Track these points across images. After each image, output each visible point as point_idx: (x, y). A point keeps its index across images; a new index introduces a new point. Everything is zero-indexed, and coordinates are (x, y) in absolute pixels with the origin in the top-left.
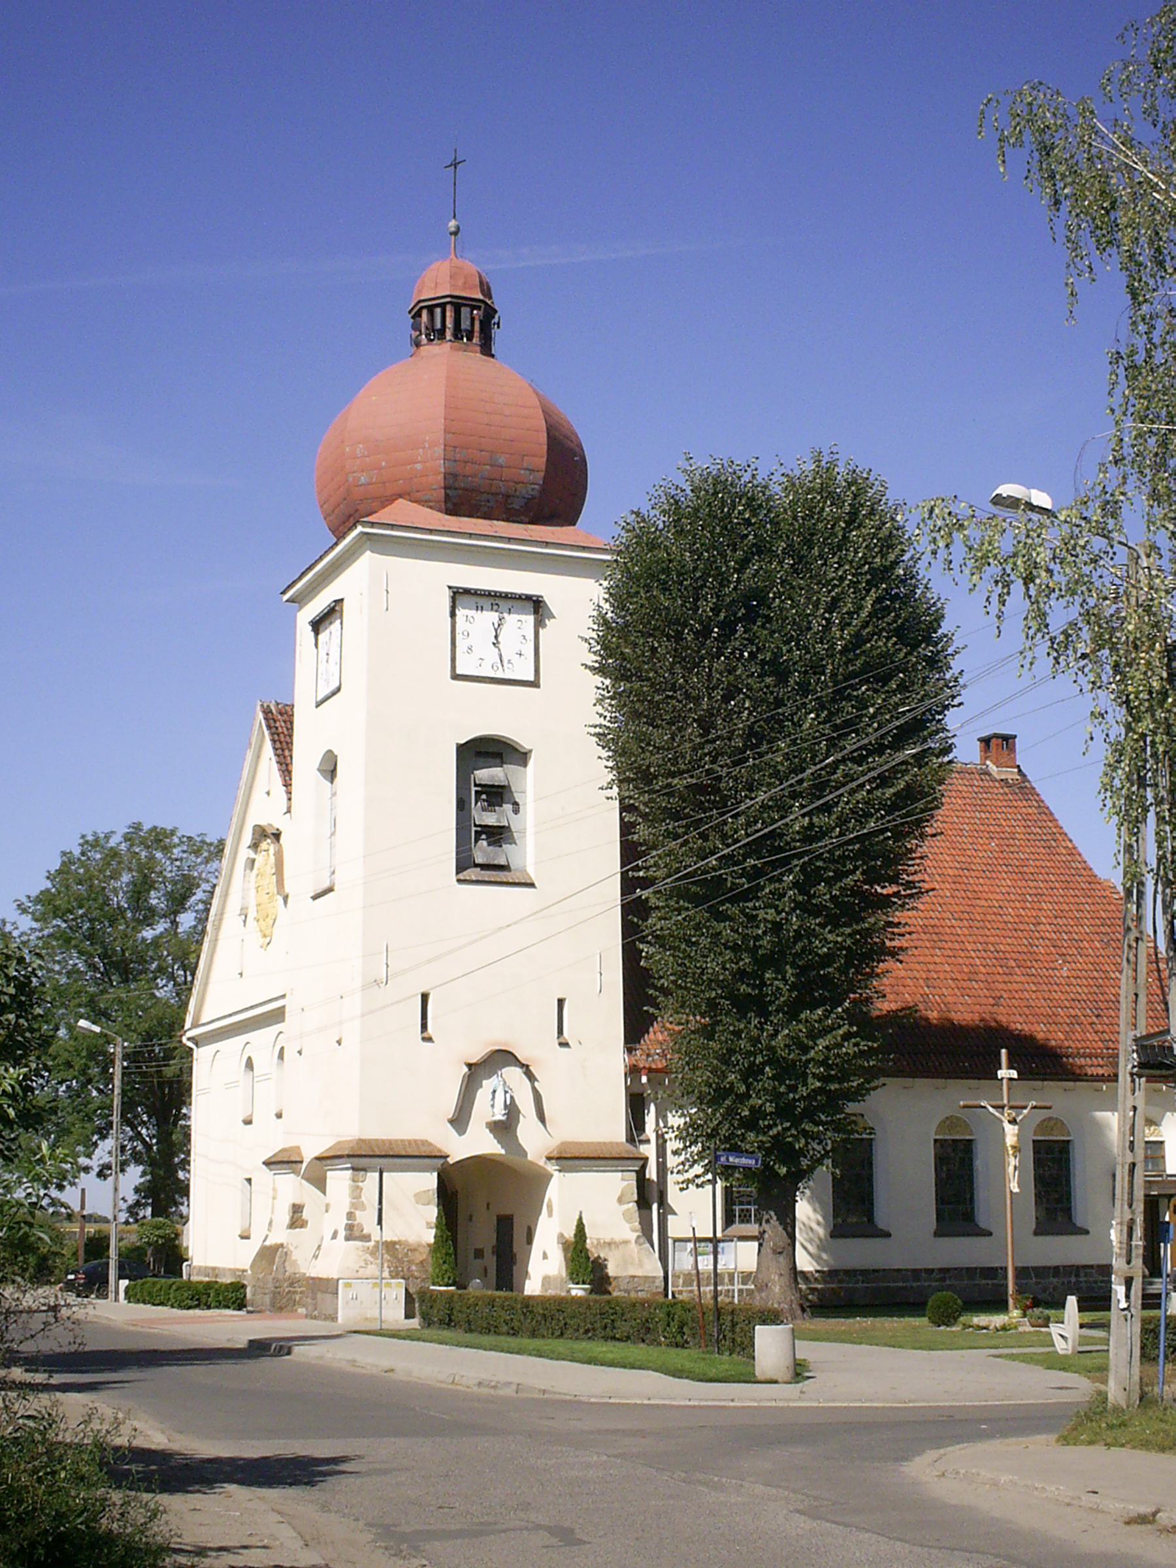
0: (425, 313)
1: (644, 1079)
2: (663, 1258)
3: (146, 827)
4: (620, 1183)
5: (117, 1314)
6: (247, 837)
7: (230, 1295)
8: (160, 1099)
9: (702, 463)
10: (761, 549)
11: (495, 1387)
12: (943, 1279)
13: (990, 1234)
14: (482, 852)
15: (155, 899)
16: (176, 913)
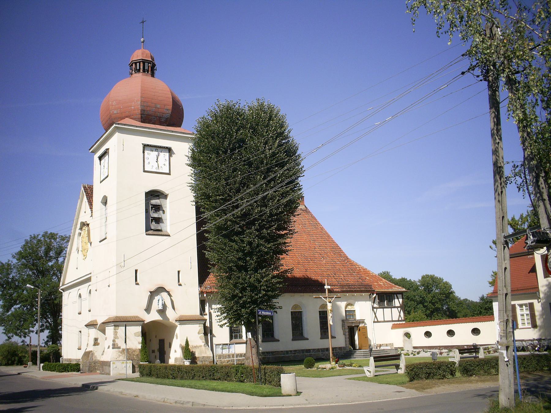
0: (134, 65)
1: (205, 295)
2: (212, 350)
3: (49, 233)
4: (198, 328)
5: (37, 374)
6: (79, 226)
7: (75, 367)
8: (53, 310)
9: (223, 102)
10: (243, 127)
11: (183, 404)
12: (295, 353)
13: (308, 339)
14: (153, 225)
15: (52, 254)
16: (58, 257)
